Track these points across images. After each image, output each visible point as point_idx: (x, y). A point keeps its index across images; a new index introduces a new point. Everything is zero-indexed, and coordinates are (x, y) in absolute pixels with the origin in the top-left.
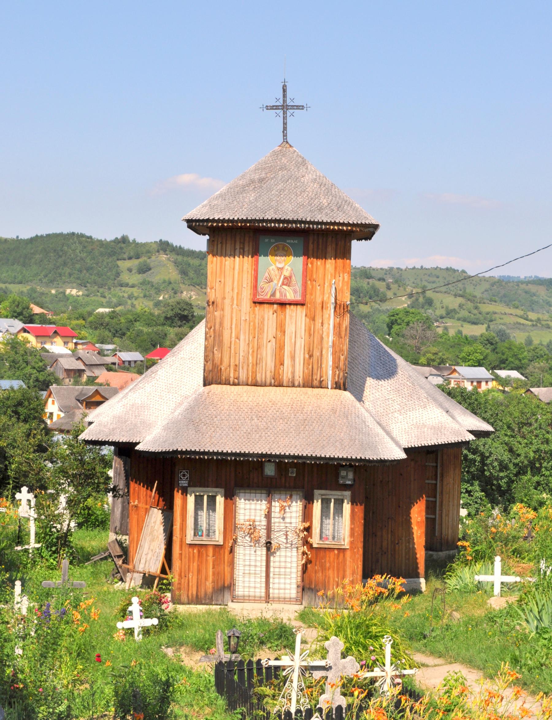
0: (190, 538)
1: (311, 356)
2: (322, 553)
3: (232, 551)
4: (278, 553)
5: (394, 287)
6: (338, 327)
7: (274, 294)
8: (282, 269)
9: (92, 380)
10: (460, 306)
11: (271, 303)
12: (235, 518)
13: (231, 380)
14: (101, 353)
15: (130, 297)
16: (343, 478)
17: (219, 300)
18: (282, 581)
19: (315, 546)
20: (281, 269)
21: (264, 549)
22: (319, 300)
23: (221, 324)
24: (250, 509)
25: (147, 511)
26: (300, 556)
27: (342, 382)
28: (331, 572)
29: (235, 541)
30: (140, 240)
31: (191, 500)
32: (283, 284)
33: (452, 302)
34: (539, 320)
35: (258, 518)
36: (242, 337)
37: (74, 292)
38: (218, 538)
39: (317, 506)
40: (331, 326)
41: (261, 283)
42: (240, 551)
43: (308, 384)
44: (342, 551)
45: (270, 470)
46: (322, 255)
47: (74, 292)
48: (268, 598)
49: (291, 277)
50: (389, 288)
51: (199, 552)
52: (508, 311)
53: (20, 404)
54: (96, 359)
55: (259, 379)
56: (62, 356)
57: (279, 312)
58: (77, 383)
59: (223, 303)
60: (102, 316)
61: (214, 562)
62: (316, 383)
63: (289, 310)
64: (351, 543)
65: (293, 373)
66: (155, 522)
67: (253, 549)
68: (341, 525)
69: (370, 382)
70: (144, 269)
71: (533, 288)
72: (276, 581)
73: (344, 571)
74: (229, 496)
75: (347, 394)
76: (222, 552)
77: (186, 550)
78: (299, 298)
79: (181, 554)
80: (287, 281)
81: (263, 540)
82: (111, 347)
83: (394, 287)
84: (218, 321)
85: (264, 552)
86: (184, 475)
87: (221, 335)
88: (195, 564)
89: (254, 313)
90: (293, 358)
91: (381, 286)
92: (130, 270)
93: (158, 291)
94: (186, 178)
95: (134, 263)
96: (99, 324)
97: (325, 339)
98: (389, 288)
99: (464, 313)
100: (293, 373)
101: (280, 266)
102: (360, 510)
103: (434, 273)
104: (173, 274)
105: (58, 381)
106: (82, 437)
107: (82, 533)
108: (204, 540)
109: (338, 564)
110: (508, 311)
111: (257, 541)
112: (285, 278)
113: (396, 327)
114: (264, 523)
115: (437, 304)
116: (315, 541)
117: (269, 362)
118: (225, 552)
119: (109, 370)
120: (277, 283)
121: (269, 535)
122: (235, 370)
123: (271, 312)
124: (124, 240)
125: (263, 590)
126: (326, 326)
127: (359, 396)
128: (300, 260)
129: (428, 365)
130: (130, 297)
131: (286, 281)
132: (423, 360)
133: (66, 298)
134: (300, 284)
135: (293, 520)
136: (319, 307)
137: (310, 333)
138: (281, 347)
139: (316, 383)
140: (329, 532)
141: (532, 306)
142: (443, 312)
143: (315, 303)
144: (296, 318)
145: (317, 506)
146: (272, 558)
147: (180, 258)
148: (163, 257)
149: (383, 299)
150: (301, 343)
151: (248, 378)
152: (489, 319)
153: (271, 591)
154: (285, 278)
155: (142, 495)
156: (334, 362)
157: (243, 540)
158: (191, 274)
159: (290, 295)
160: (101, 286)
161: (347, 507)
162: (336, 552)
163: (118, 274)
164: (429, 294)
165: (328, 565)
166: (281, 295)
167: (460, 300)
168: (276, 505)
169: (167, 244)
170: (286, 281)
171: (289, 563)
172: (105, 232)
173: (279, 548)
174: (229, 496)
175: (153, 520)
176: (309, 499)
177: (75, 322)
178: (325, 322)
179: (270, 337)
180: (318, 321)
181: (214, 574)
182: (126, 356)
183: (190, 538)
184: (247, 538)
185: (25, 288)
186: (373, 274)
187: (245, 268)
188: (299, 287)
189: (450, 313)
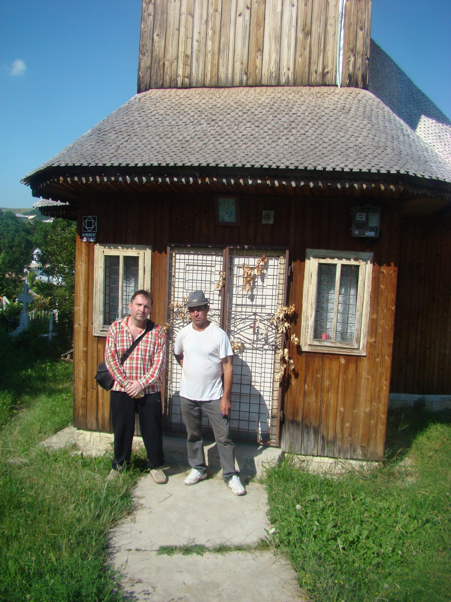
1: (308, 33)
2: (317, 362)
13: (180, 80)
24: (196, 272)
28: (331, 396)
55: (222, 76)
62: (315, 78)
64: (371, 346)
73: (356, 395)
79: (86, 352)
86: (90, 224)
90: (279, 39)
109: (345, 382)
122: (185, 64)
151: (205, 75)
162: (343, 361)
165: (327, 383)
176: (297, 258)
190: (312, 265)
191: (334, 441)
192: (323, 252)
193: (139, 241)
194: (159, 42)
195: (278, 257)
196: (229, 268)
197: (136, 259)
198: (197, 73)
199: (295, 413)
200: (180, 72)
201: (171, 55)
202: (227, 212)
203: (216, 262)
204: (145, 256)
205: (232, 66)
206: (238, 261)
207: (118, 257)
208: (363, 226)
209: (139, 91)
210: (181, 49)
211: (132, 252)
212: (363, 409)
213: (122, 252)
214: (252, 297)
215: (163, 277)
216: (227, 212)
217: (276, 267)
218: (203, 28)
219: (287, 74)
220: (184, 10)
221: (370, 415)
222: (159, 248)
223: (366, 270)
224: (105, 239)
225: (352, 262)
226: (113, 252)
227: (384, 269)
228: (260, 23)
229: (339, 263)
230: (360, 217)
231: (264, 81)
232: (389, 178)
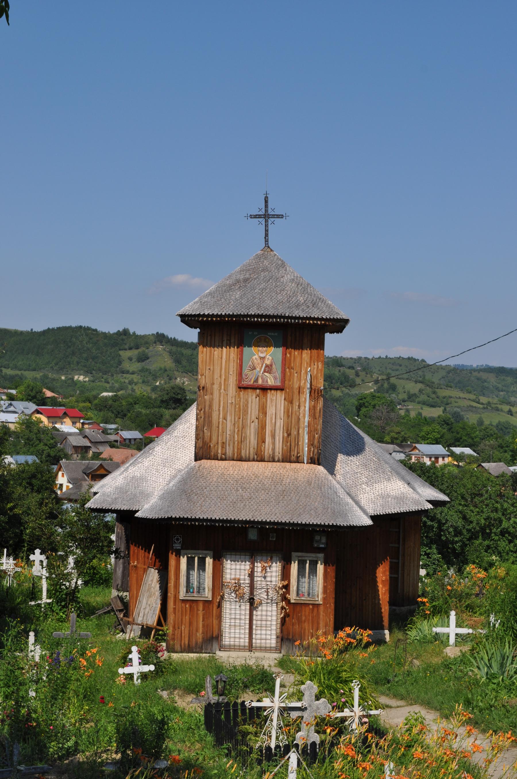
3: (220, 606)
4: (260, 608)
5: (362, 374)
6: (313, 409)
7: (256, 380)
8: (263, 359)
9: (97, 456)
10: (421, 391)
12: (222, 577)
13: (219, 455)
14: (105, 432)
15: (131, 383)
16: (317, 541)
17: (208, 385)
18: (264, 632)
22: (296, 386)
23: (210, 406)
25: (145, 571)
26: (279, 611)
27: (316, 457)
29: (222, 597)
30: (139, 333)
31: (184, 561)
32: (265, 371)
33: (413, 387)
34: (489, 403)
35: (242, 577)
36: (229, 418)
37: (81, 378)
38: (208, 594)
39: (294, 567)
43: (287, 459)
44: (316, 606)
45: (253, 535)
46: (299, 346)
47: (81, 378)
48: (251, 648)
49: (271, 365)
50: (357, 375)
52: (462, 395)
53: (34, 476)
54: (100, 437)
55: (243, 454)
56: (71, 434)
57: (261, 396)
58: (83, 458)
59: (212, 389)
60: (106, 398)
61: (203, 616)
62: (293, 458)
63: (270, 395)
64: (324, 599)
65: (274, 449)
66: (152, 581)
67: (238, 604)
68: (315, 584)
69: (341, 457)
71: (484, 375)
72: (259, 632)
73: (318, 624)
74: (218, 558)
76: (211, 607)
77: (179, 605)
78: (278, 383)
79: (175, 609)
80: (269, 369)
81: (247, 597)
82: (113, 426)
83: (362, 374)
84: (207, 403)
86: (178, 539)
88: (187, 617)
89: (239, 397)
90: (273, 436)
91: (351, 373)
92: (130, 359)
93: (155, 378)
94: (180, 278)
96: (104, 406)
98: (357, 375)
99: (423, 397)
100: (274, 449)
101: (262, 355)
102: (332, 570)
103: (398, 362)
104: (168, 362)
105: (67, 457)
106: (88, 505)
107: (87, 590)
108: (195, 596)
109: (313, 617)
110: (462, 395)
112: (267, 366)
113: (363, 410)
115: (400, 390)
116: (293, 597)
118: (214, 607)
119: (112, 446)
120: (260, 370)
122: (222, 447)
123: (254, 396)
124: (125, 332)
126: (302, 408)
127: (331, 470)
129: (392, 443)
130: (131, 383)
131: (267, 369)
132: (387, 438)
133: (75, 383)
135: (274, 579)
136: (296, 392)
137: (288, 414)
138: (262, 427)
139: (293, 458)
140: (305, 588)
141: (483, 391)
142: (405, 396)
144: (276, 403)
145: (294, 567)
146: (255, 612)
147: (174, 349)
148: (160, 348)
149: (353, 385)
150: (280, 424)
151: (234, 454)
152: (445, 402)
153: (254, 641)
154: (267, 366)
155: (140, 556)
157: (229, 596)
158: (184, 363)
159: (271, 382)
160: (105, 373)
161: (320, 568)
162: (311, 607)
163: (120, 363)
164: (393, 380)
165: (304, 618)
166: (263, 381)
167: (420, 386)
168: (258, 566)
169: (163, 335)
170: (267, 369)
171: (270, 615)
172: (108, 326)
173: (261, 604)
174: (218, 558)
175: (150, 579)
177: (82, 405)
179: (253, 418)
182: (127, 434)
183: (182, 594)
184: (233, 594)
185: (38, 375)
186: (344, 362)
187: (231, 357)
188: (278, 374)
189: (411, 398)
199: (288, 634)
200: (220, 451)
202: (253, 535)
210: (220, 439)
218: (232, 428)
220: (221, 416)
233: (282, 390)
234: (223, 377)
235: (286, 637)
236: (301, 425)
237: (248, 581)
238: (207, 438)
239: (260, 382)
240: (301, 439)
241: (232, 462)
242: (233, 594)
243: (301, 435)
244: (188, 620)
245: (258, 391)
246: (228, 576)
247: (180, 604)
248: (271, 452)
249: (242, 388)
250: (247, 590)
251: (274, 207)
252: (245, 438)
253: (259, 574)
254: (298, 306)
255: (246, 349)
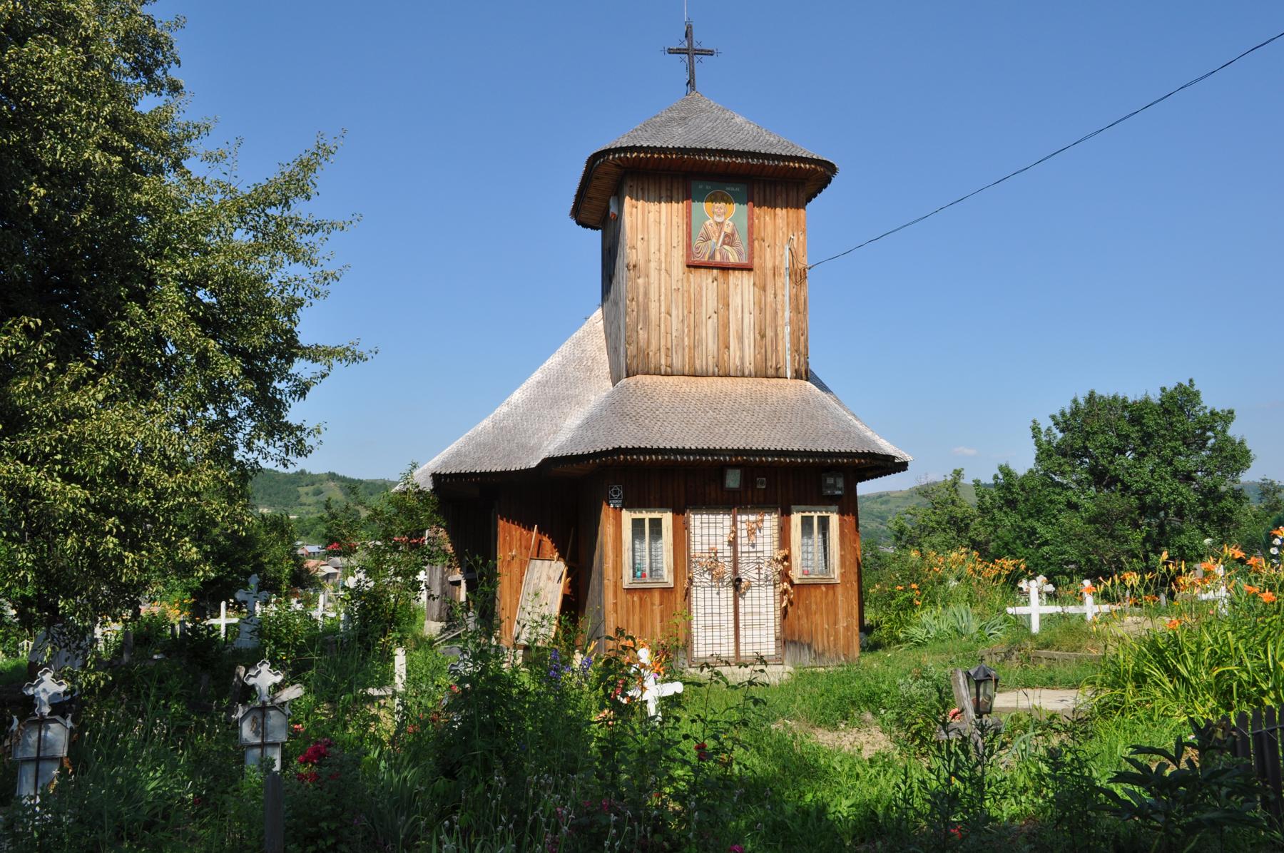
0: (627, 580)
1: (763, 336)
2: (805, 592)
3: (687, 593)
4: (748, 594)
7: (713, 256)
11: (709, 267)
12: (689, 548)
13: (663, 369)
16: (829, 487)
17: (641, 263)
18: (756, 632)
19: (796, 582)
20: (720, 224)
21: (731, 591)
22: (769, 265)
23: (646, 294)
24: (710, 530)
25: (523, 565)
26: (778, 597)
27: (803, 369)
28: (818, 617)
29: (691, 580)
32: (724, 243)
35: (719, 547)
36: (674, 313)
38: (668, 578)
40: (787, 298)
41: (696, 242)
42: (698, 595)
44: (831, 586)
49: (733, 235)
51: (641, 599)
55: (698, 367)
57: (721, 280)
59: (647, 268)
61: (662, 612)
62: (771, 372)
63: (734, 277)
64: (843, 575)
65: (742, 358)
66: (539, 578)
67: (715, 590)
70: (318, 493)
72: (749, 632)
73: (836, 615)
75: (808, 384)
76: (672, 597)
77: (623, 597)
78: (744, 261)
79: (615, 604)
80: (729, 239)
81: (728, 577)
84: (641, 290)
85: (731, 594)
86: (616, 492)
87: (646, 309)
88: (637, 618)
89: (688, 280)
90: (741, 339)
95: (311, 488)
97: (780, 314)
100: (742, 358)
101: (719, 220)
108: (648, 583)
109: (827, 605)
111: (721, 579)
112: (726, 235)
114: (728, 552)
116: (796, 575)
117: (711, 345)
118: (676, 597)
120: (716, 241)
121: (735, 571)
122: (667, 356)
123: (710, 280)
125: (732, 647)
126: (779, 297)
128: (744, 208)
131: (727, 240)
134: (745, 243)
135: (767, 548)
136: (769, 273)
139: (771, 372)
143: (764, 268)
144: (741, 285)
146: (741, 602)
148: (332, 484)
151: (684, 366)
153: (742, 647)
154: (726, 235)
156: (792, 344)
157: (702, 579)
159: (733, 258)
162: (824, 589)
163: (299, 497)
165: (814, 607)
166: (722, 257)
170: (727, 240)
171: (763, 605)
173: (749, 587)
175: (536, 575)
176: (786, 513)
178: (779, 292)
179: (711, 311)
180: (770, 292)
181: (662, 630)
183: (627, 580)
184: (706, 575)
187: (674, 223)
188: (744, 247)
190: (796, 519)
191: (823, 654)
192: (803, 507)
193: (662, 505)
194: (642, 334)
195: (770, 514)
196: (735, 523)
197: (660, 520)
198: (677, 363)
199: (793, 634)
200: (663, 362)
201: (653, 347)
202: (733, 480)
203: (724, 520)
204: (667, 518)
205: (706, 358)
206: (739, 518)
207: (643, 520)
208: (834, 486)
209: (628, 376)
210: (663, 343)
211: (656, 515)
212: (842, 624)
213: (646, 515)
214: (753, 545)
215: (681, 533)
216: (733, 480)
217: (770, 522)
218: (680, 326)
219: (749, 367)
220: (663, 309)
221: (847, 628)
222: (678, 511)
223: (834, 519)
224: (630, 504)
225: (824, 514)
226: (638, 516)
227: (846, 518)
228: (726, 325)
229: (816, 515)
230: (830, 481)
231: (732, 373)
232: (857, 455)
233: (750, 269)
234: (663, 250)
235: (789, 639)
236: (780, 322)
237: (727, 554)
238: (642, 343)
239: (718, 258)
240: (780, 343)
241: (682, 378)
242: (706, 575)
243: (780, 336)
244: (637, 622)
245: (715, 271)
246: (698, 547)
247: (624, 595)
248: (738, 362)
249: (692, 266)
250: (728, 568)
251: (702, 39)
252: (700, 341)
253: (745, 541)
254: (771, 144)
255: (696, 206)
